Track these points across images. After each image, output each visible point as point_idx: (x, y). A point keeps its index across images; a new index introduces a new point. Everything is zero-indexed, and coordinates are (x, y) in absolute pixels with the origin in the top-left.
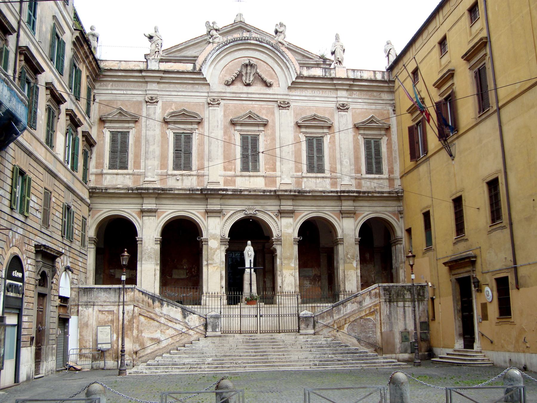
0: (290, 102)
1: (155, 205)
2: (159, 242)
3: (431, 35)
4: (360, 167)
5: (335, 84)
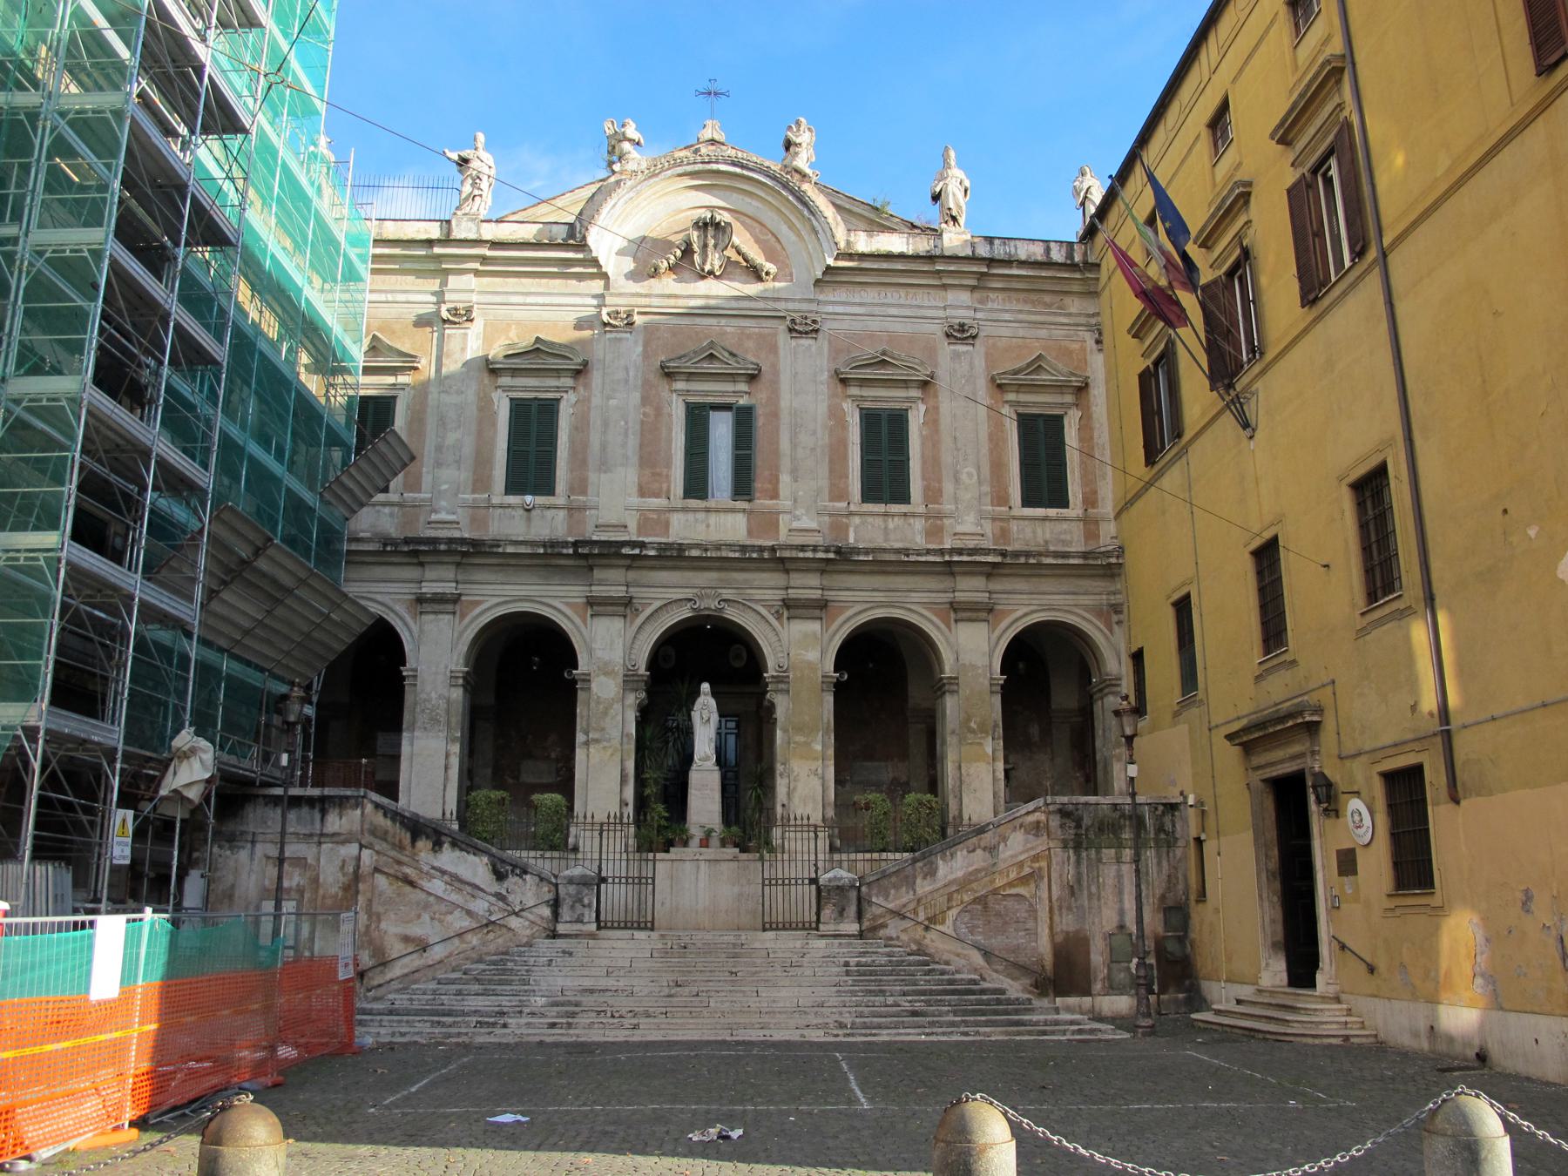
0: (819, 319)
1: (454, 585)
2: (461, 681)
3: (1187, 110)
5: (939, 272)
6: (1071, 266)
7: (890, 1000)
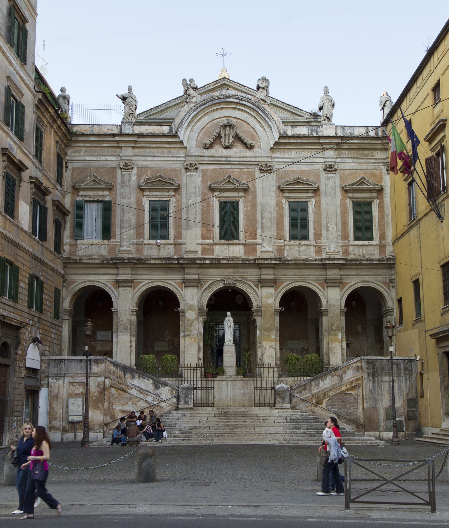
0: (272, 165)
1: (131, 276)
2: (135, 313)
3: (425, 81)
4: (348, 233)
5: (321, 143)
6: (377, 138)
7: (303, 431)
